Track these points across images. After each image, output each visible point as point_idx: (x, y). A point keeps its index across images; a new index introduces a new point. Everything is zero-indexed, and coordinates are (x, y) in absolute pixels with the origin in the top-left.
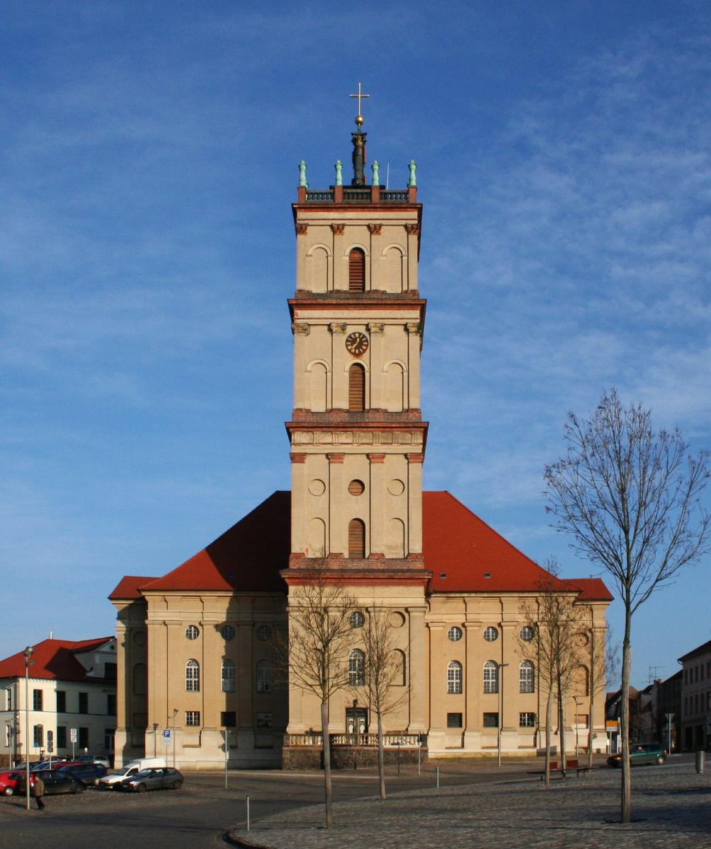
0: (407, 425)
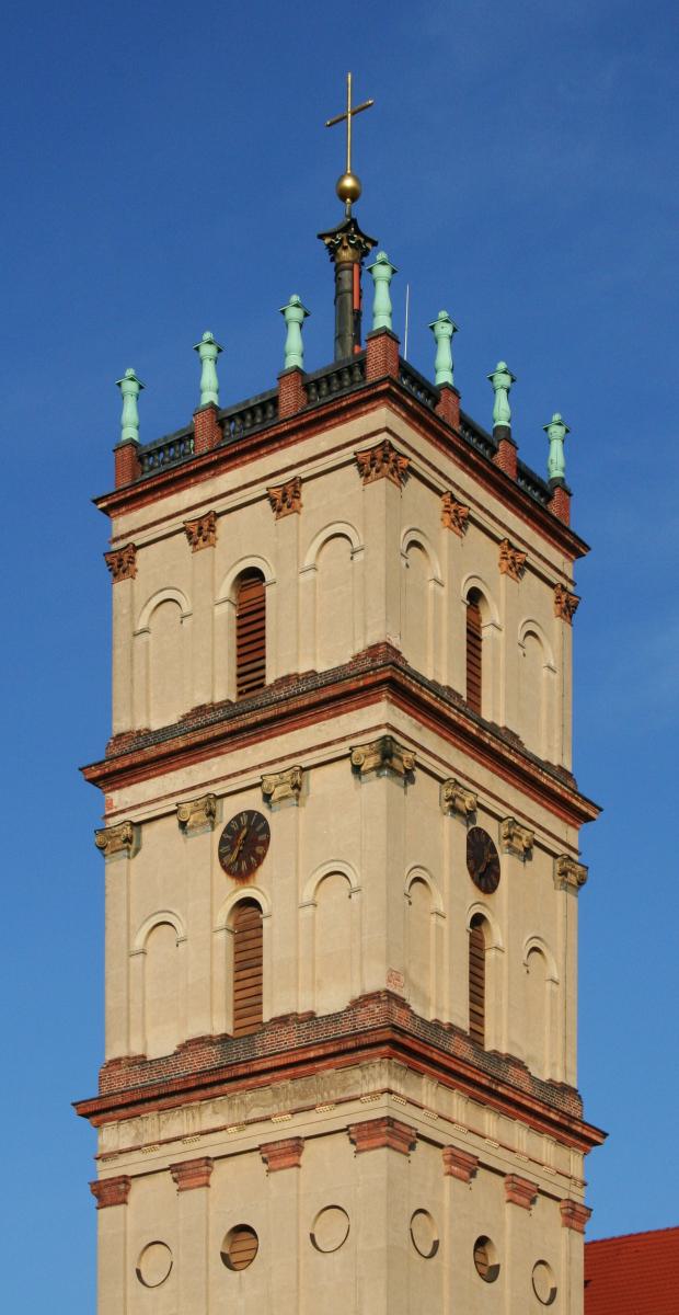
0: (342, 1047)
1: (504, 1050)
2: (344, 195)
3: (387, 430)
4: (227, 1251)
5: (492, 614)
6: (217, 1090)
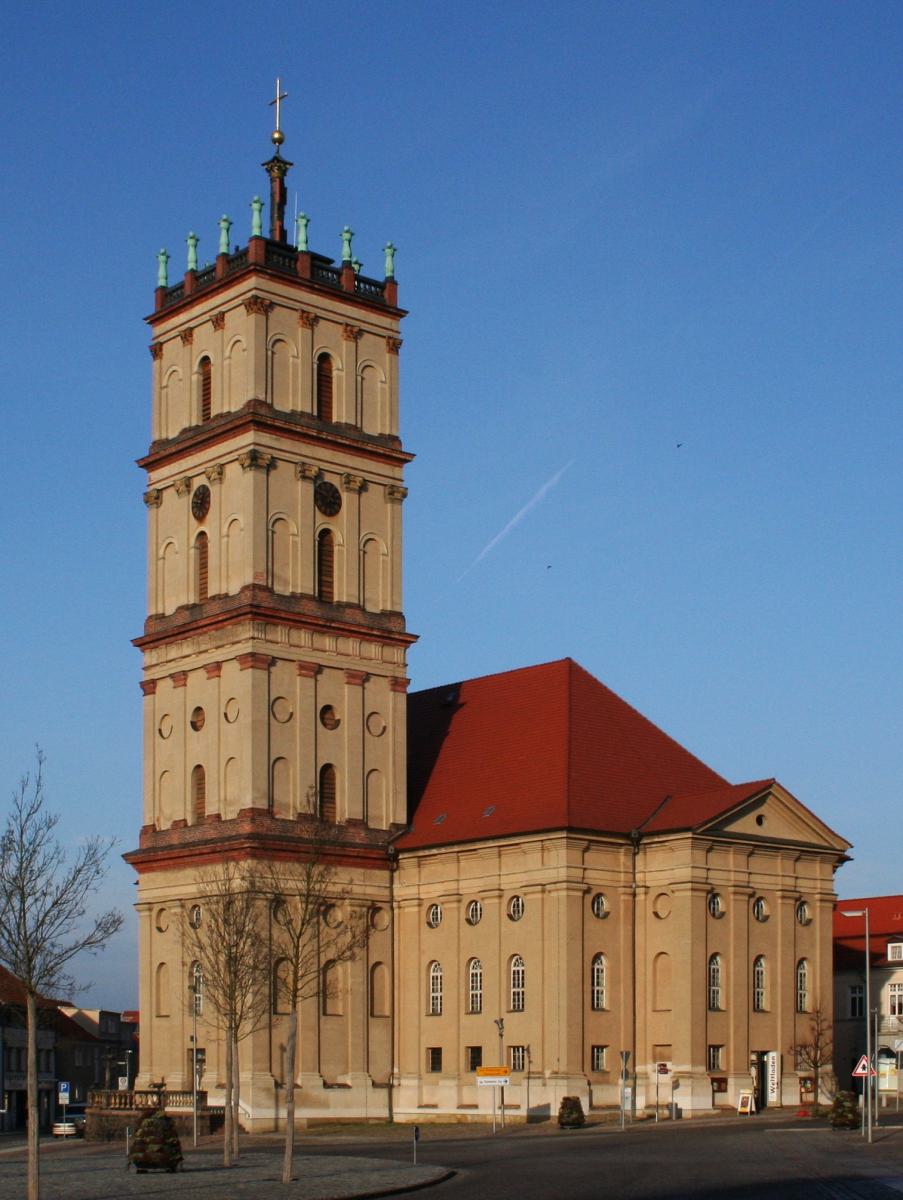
1: (345, 600)
2: (275, 141)
3: (256, 288)
4: (195, 720)
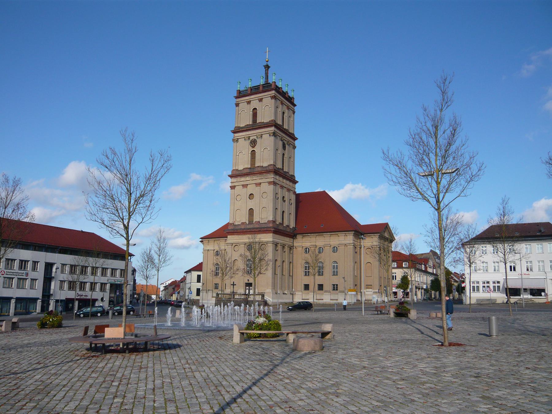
5: (286, 115)
6: (524, 313)
